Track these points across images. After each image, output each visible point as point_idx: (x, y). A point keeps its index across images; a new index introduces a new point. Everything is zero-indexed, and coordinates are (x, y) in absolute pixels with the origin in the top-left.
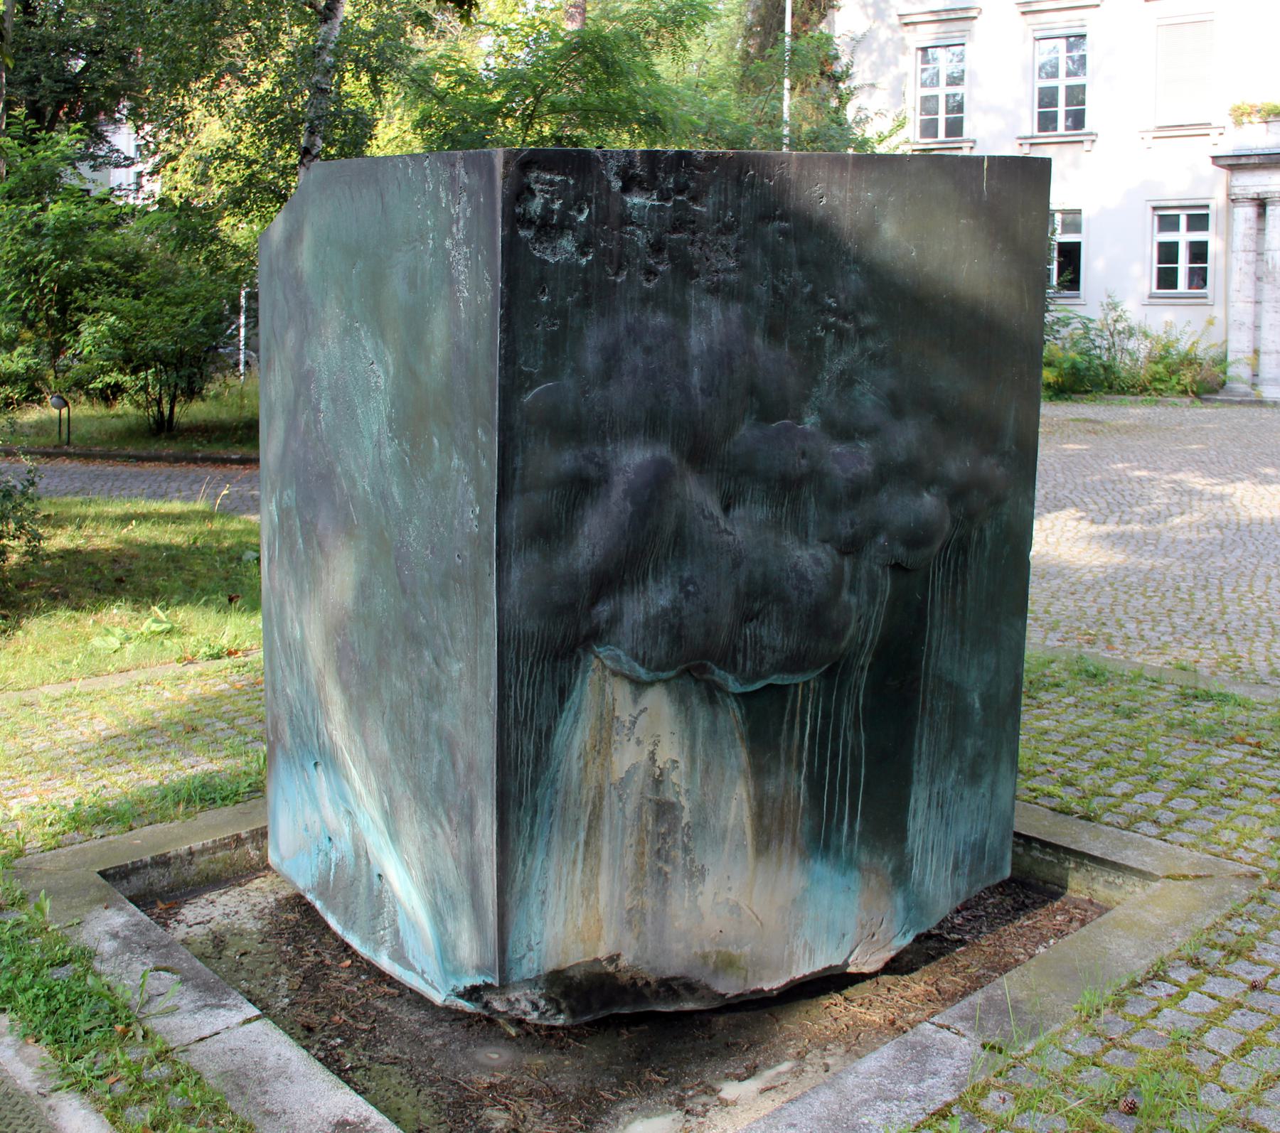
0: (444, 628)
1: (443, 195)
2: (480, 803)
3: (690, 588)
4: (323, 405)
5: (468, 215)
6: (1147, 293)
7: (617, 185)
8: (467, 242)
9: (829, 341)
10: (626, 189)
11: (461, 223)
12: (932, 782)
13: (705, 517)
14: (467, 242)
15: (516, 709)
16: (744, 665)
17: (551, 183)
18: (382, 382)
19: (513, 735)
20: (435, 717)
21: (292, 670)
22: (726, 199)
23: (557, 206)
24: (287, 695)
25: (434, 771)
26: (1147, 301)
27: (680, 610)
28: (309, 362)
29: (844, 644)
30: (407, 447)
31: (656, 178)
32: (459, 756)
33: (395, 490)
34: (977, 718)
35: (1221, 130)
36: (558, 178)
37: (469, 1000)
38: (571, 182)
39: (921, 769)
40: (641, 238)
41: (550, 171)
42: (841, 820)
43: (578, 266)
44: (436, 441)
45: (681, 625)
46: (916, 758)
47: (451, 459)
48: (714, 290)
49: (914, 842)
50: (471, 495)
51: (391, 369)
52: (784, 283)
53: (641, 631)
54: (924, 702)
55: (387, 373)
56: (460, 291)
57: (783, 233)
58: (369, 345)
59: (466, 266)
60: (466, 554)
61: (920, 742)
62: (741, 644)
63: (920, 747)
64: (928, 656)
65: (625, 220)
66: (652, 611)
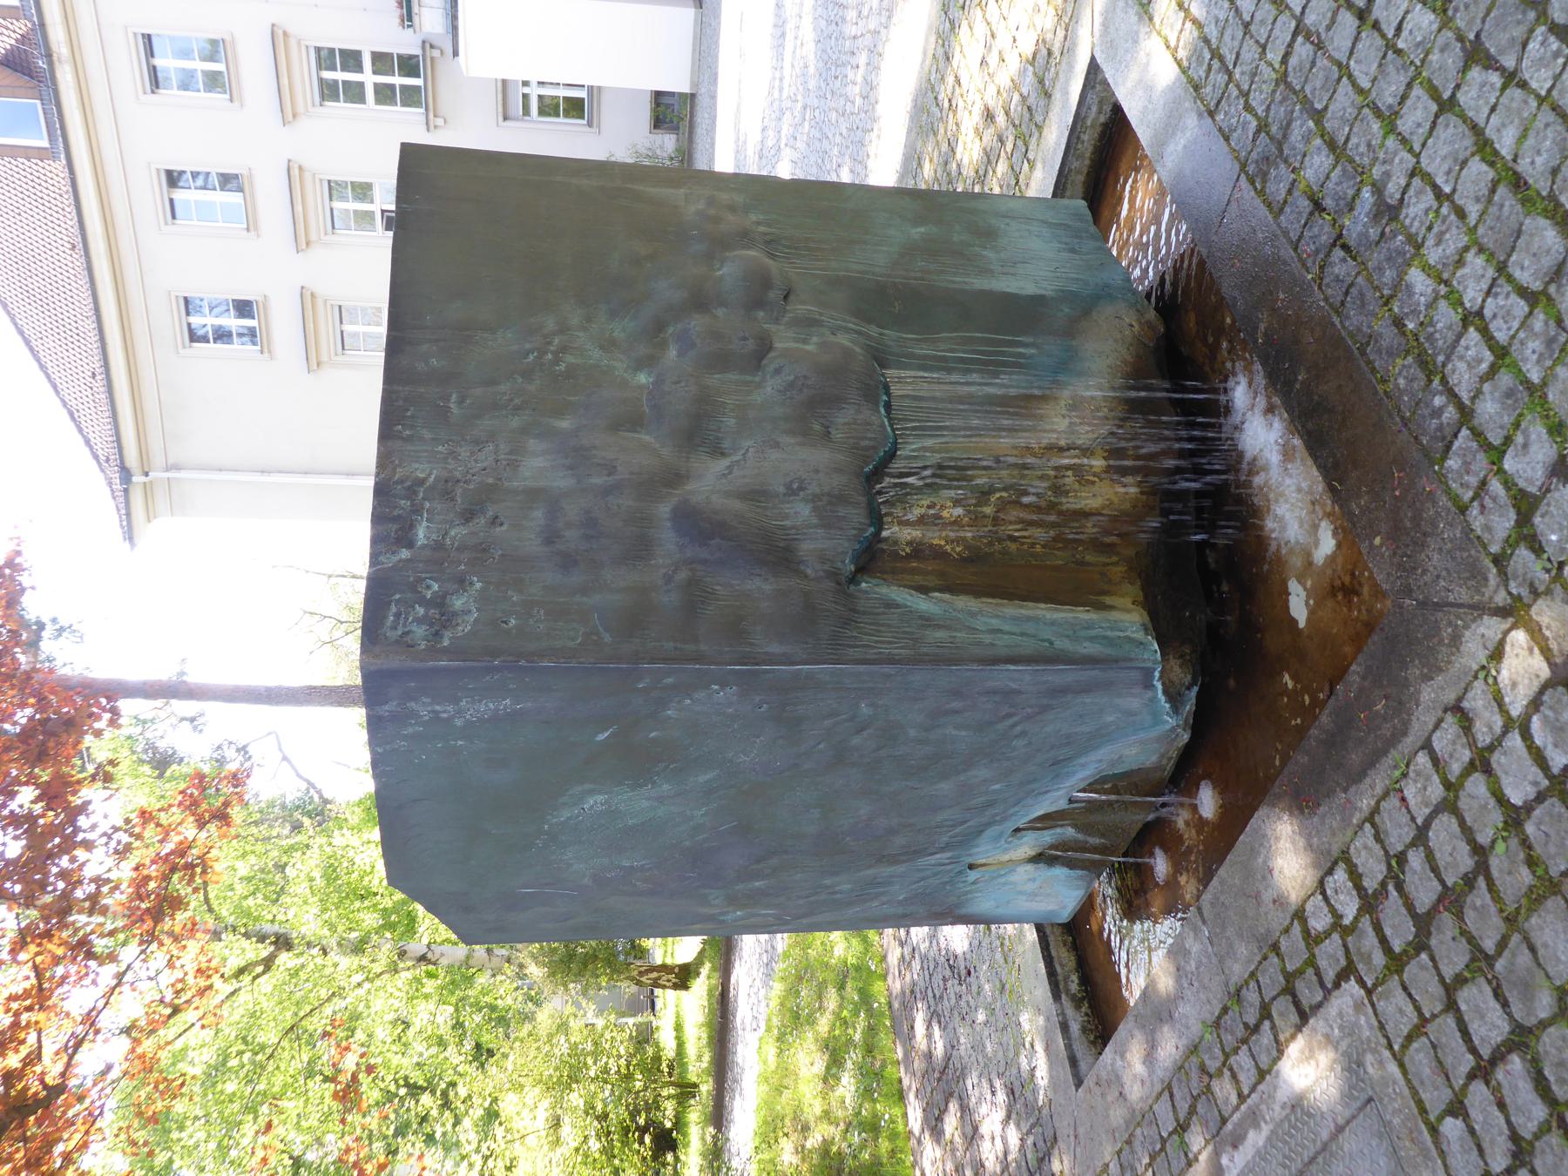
0: (828, 723)
1: (411, 730)
2: (990, 684)
3: (795, 486)
4: (626, 863)
5: (429, 700)
6: (588, 129)
7: (405, 554)
8: (456, 701)
9: (570, 359)
10: (410, 545)
11: (438, 708)
12: (991, 271)
13: (730, 473)
14: (456, 701)
15: (901, 648)
16: (870, 439)
17: (398, 615)
18: (600, 798)
19: (925, 650)
20: (912, 733)
21: (881, 894)
22: (426, 451)
23: (421, 611)
24: (906, 899)
25: (963, 733)
26: (595, 129)
27: (815, 496)
28: (586, 881)
29: (858, 350)
30: (661, 765)
31: (399, 516)
32: (947, 706)
33: (702, 778)
34: (935, 229)
35: (428, 46)
36: (393, 609)
37: (1183, 704)
38: (397, 596)
39: (980, 283)
40: (458, 532)
41: (385, 617)
42: (1021, 355)
43: (483, 590)
44: (652, 735)
45: (829, 494)
46: (967, 287)
47: (669, 718)
48: (514, 465)
49: (1045, 289)
50: (700, 695)
51: (587, 786)
52: (512, 400)
53: (833, 531)
54: (916, 279)
55: (592, 792)
56: (505, 709)
57: (461, 402)
58: (565, 814)
59: (480, 701)
60: (758, 699)
61: (954, 282)
62: (852, 441)
63: (959, 282)
64: (873, 274)
65: (438, 546)
66: (815, 521)
